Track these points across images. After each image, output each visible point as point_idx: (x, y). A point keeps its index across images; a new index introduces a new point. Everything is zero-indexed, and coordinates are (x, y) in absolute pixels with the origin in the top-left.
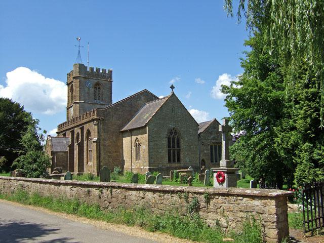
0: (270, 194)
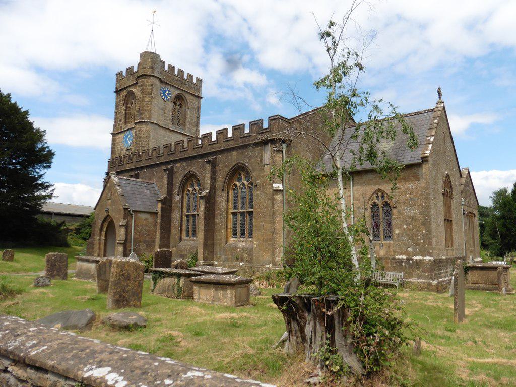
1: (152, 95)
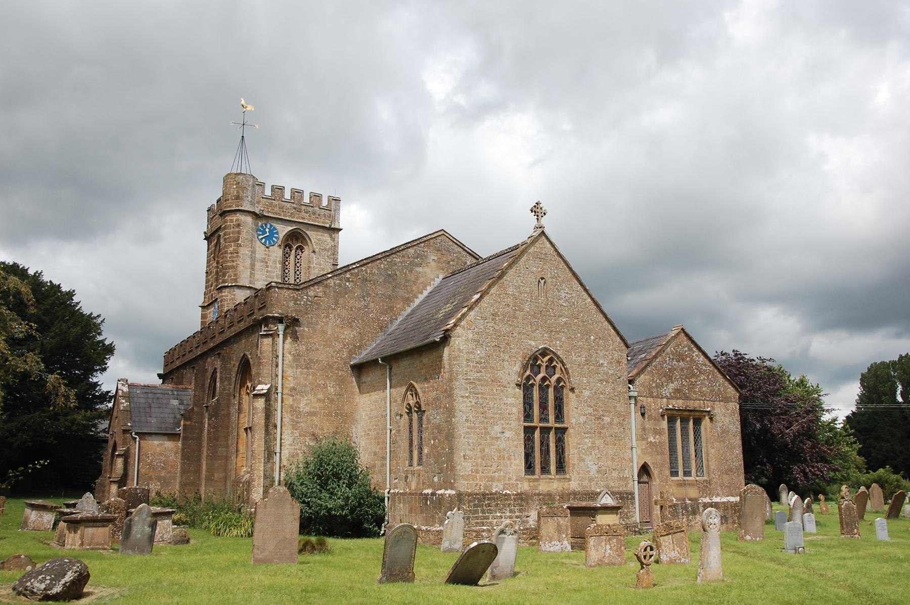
1: (240, 242)
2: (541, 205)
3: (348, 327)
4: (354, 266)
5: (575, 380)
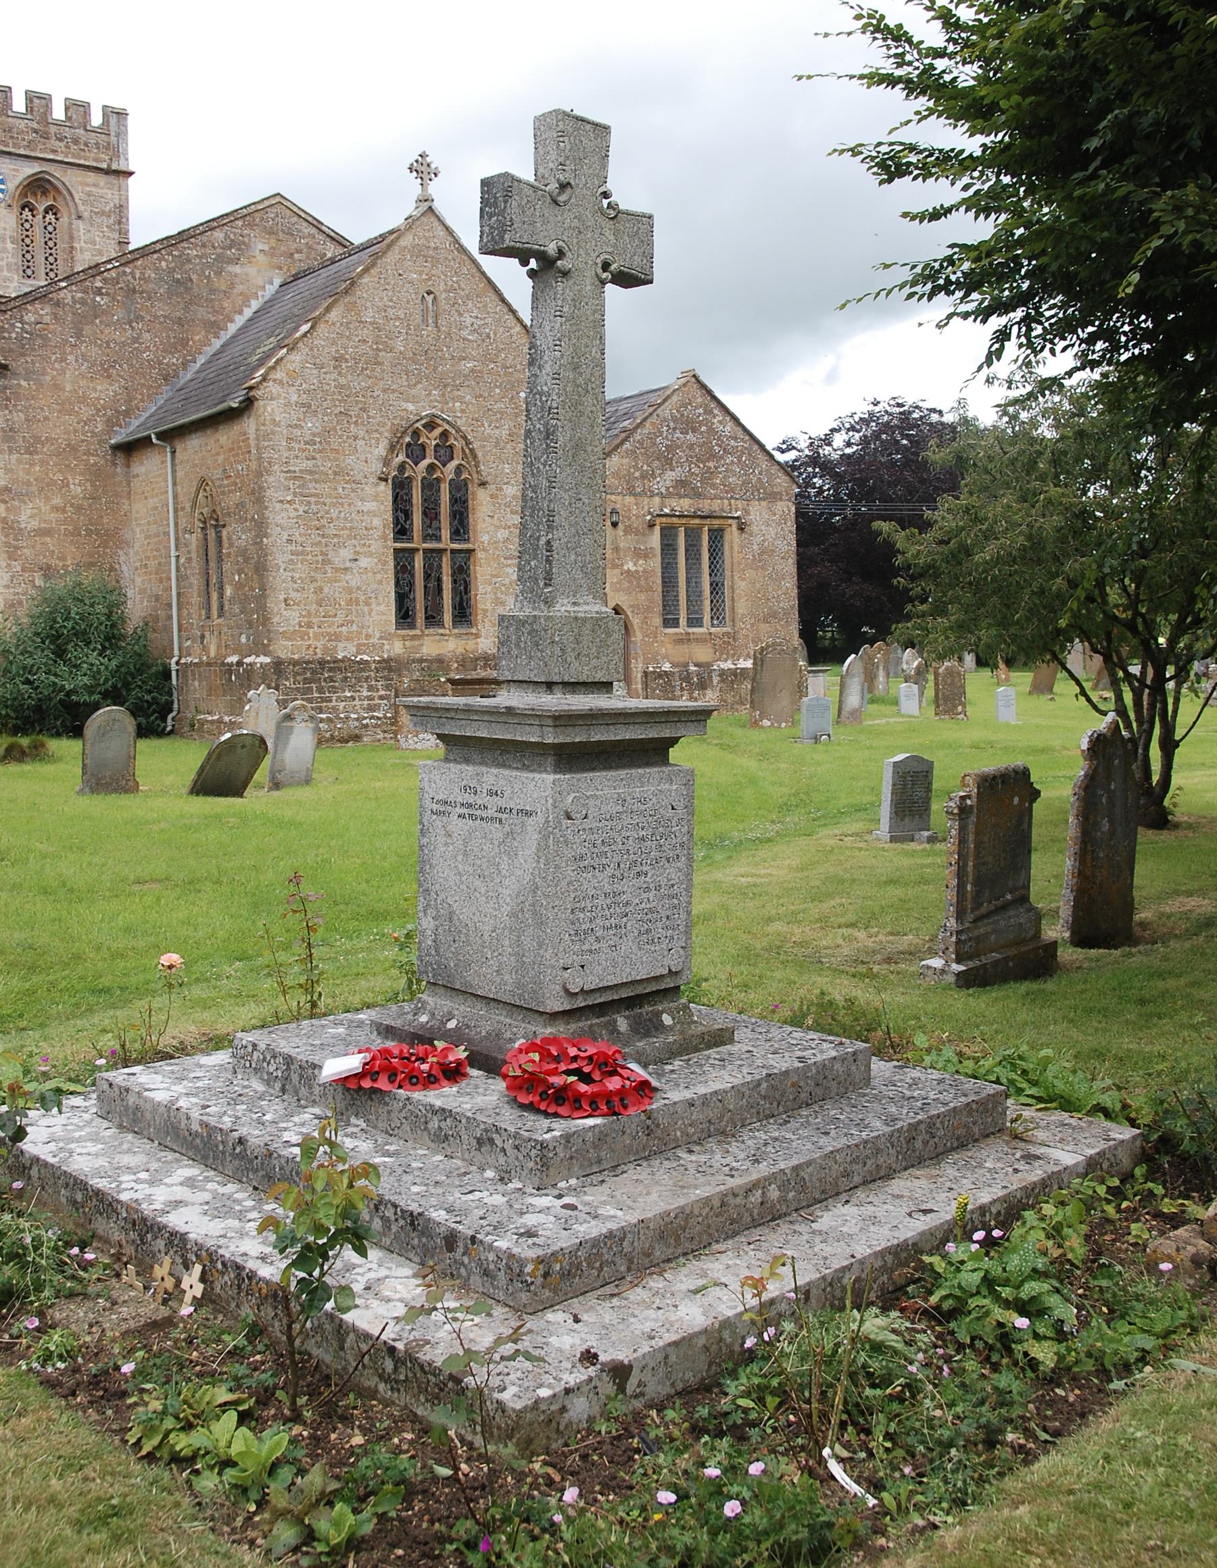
0: (884, 526)
2: (428, 159)
3: (102, 376)
4: (109, 266)
5: (487, 469)
